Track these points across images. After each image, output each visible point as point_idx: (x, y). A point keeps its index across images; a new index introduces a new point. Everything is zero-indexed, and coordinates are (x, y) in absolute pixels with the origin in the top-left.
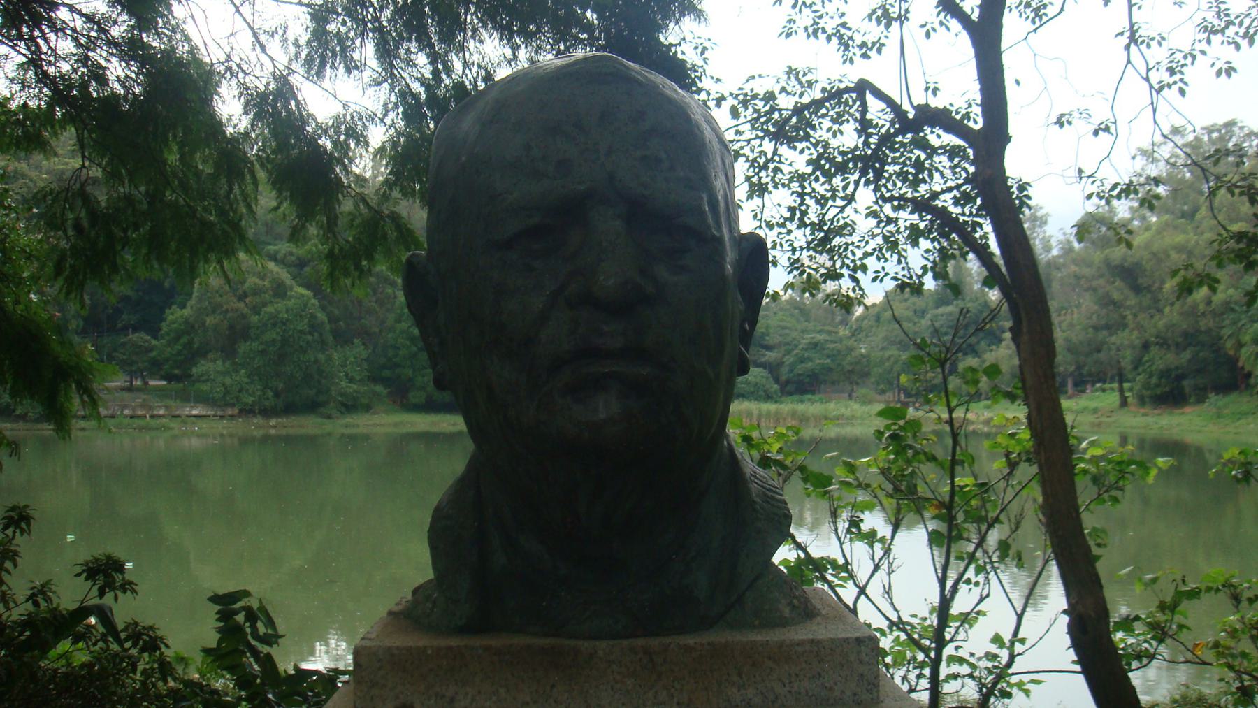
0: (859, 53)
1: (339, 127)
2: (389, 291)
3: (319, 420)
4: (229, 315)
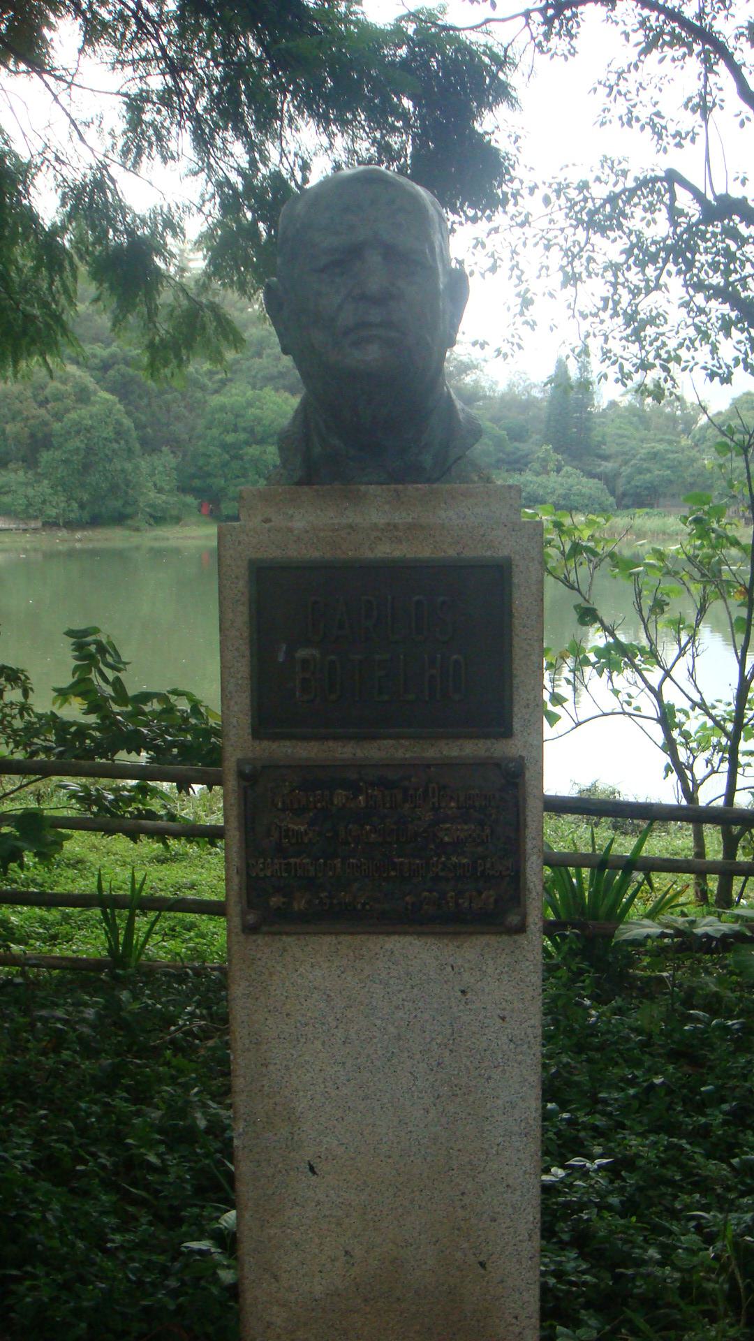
0: (673, 142)
1: (155, 218)
2: (199, 394)
3: (127, 533)
4: (32, 421)
